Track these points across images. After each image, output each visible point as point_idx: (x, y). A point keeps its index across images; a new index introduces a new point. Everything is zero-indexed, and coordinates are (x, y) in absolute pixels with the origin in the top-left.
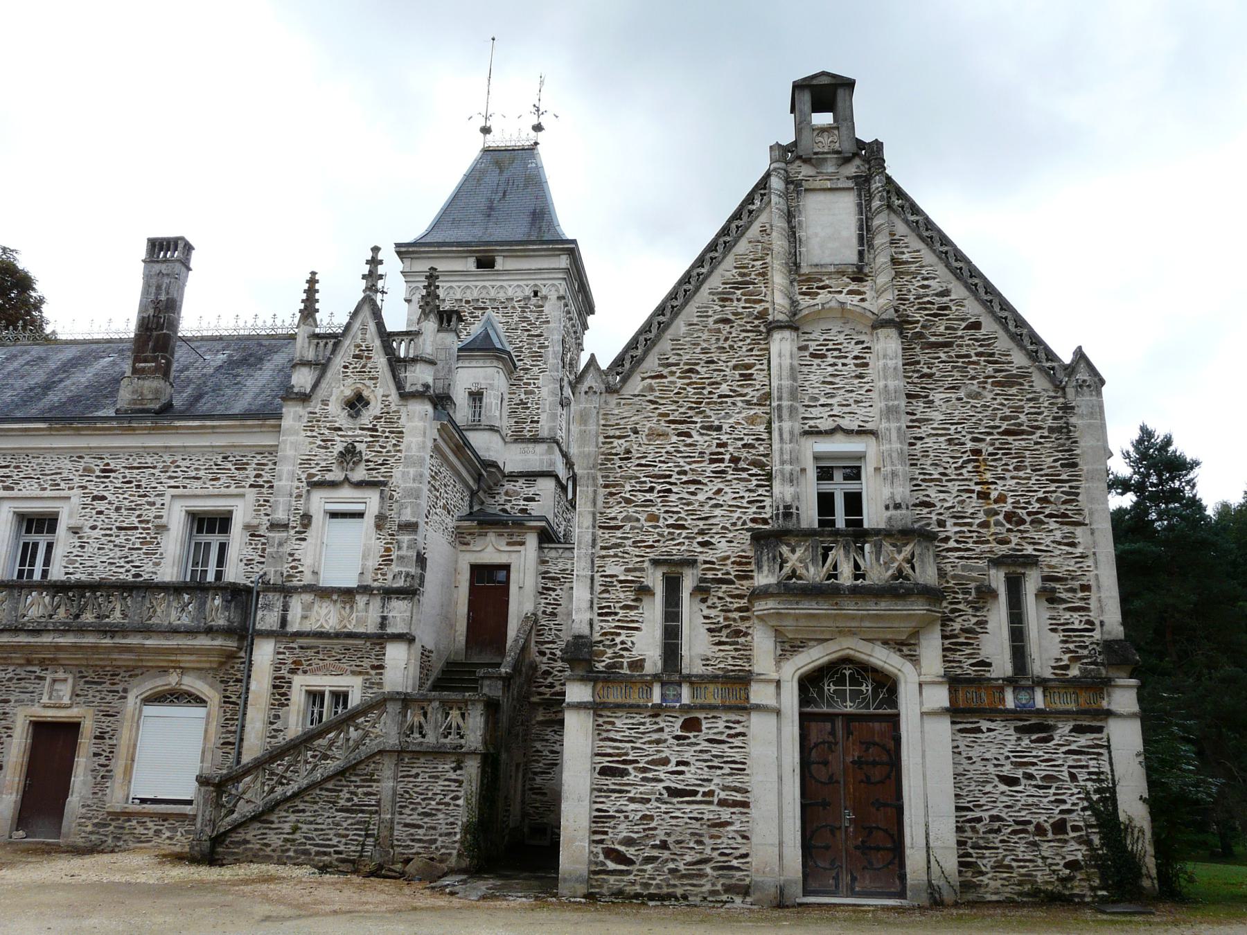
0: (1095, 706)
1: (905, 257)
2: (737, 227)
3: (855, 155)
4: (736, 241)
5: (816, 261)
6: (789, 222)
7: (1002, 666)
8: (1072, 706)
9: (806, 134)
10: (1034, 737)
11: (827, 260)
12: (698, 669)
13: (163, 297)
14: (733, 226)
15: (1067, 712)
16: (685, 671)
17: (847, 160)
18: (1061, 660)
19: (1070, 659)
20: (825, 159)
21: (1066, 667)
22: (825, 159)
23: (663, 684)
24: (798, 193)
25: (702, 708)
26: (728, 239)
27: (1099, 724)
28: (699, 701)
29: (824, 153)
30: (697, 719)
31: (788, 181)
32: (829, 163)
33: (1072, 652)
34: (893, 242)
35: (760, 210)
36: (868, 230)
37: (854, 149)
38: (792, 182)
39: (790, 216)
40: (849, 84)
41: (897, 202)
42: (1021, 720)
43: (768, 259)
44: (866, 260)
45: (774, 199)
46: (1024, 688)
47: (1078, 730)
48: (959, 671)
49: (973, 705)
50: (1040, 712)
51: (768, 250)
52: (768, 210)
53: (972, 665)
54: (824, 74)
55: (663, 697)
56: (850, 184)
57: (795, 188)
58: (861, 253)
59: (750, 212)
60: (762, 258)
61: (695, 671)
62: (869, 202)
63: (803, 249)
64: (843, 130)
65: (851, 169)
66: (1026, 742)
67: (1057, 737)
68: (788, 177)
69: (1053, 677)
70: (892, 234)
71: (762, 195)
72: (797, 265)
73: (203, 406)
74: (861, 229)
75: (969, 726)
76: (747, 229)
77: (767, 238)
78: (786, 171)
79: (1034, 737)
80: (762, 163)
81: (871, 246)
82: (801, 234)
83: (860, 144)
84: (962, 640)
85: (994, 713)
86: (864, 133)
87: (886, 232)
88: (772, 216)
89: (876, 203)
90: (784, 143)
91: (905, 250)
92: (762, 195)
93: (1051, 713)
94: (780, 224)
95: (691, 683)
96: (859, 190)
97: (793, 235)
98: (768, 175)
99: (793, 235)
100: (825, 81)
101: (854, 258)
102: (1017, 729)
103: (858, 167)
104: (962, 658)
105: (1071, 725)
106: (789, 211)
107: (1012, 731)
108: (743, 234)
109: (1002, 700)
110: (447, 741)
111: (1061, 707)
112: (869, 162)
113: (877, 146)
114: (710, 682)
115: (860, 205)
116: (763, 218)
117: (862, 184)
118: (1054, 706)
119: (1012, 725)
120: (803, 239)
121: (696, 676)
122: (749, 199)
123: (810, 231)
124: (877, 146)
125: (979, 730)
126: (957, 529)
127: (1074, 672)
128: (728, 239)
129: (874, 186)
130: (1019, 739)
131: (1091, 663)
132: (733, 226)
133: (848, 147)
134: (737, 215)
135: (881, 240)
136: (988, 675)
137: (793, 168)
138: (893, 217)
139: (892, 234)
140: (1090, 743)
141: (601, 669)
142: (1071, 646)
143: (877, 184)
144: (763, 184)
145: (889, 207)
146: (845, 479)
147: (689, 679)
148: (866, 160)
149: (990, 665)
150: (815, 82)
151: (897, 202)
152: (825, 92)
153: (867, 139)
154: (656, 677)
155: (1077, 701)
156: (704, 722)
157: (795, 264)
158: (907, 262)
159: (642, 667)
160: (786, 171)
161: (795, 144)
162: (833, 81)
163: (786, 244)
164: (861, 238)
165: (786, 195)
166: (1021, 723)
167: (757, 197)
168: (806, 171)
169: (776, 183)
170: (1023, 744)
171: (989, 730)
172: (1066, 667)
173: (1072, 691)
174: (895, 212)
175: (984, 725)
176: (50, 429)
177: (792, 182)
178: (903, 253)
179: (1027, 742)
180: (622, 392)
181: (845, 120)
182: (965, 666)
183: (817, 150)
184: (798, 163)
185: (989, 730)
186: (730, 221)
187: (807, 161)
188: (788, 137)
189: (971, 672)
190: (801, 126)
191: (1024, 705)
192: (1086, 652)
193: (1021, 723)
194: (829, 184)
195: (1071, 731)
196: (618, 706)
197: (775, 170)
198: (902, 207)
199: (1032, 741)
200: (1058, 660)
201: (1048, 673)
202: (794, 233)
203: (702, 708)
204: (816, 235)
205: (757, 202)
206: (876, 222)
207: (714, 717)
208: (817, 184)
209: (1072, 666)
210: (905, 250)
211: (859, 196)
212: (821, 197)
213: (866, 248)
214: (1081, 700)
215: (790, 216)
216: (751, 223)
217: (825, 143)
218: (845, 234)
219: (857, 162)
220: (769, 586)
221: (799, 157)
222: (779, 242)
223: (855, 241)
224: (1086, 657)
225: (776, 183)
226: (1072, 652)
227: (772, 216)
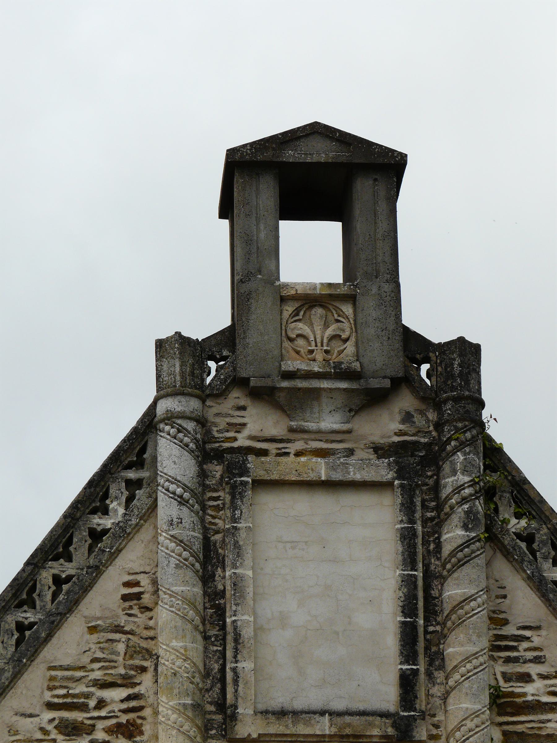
1: (533, 690)
2: (58, 581)
3: (406, 381)
4: (54, 623)
5: (279, 699)
6: (207, 579)
9: (262, 309)
11: (312, 699)
14: (46, 577)
17: (370, 400)
20: (314, 394)
22: (315, 393)
24: (236, 492)
26: (30, 616)
29: (309, 375)
31: (206, 451)
32: (326, 404)
34: (501, 645)
35: (124, 533)
36: (431, 611)
37: (396, 367)
38: (218, 455)
39: (210, 559)
40: (389, 167)
41: (516, 525)
43: (146, 683)
44: (421, 704)
45: (167, 509)
51: (144, 655)
52: (145, 534)
54: (317, 130)
56: (383, 471)
57: (228, 475)
58: (407, 683)
59: (96, 535)
60: (126, 681)
62: (435, 526)
63: (246, 665)
64: (369, 306)
65: (385, 425)
68: (208, 438)
70: (497, 620)
71: (133, 485)
72: (227, 713)
74: (408, 608)
76: (86, 589)
77: (141, 619)
78: (202, 422)
80: (132, 393)
81: (436, 659)
82: (241, 617)
83: (415, 346)
86: (428, 314)
87: (480, 620)
88: (156, 550)
89: (454, 535)
90: (199, 331)
91: (534, 669)
92: (133, 485)
94: (179, 585)
96: (408, 493)
97: (215, 619)
98: (148, 426)
99: (215, 619)
100: (320, 152)
101: (388, 697)
103: (407, 418)
106: (207, 545)
108: (73, 605)
112: (438, 406)
113: (464, 357)
115: (407, 537)
116: (132, 558)
117: (413, 470)
120: (247, 633)
122: (94, 497)
123: (268, 609)
124: (464, 357)
128: (30, 616)
129: (449, 482)
132: (46, 577)
133: (381, 359)
134: (56, 546)
135: (464, 645)
137: (222, 412)
138: (503, 569)
139: (497, 620)
143: (458, 475)
144: (135, 451)
145: (493, 536)
146: (517, 629)
148: (430, 398)
150: (290, 155)
151: (516, 525)
152: (322, 174)
153: (438, 334)
157: (221, 705)
158: (537, 707)
160: (202, 422)
161: (227, 339)
162: (344, 156)
163: (195, 647)
164: (408, 636)
165: (198, 497)
167: (118, 489)
168: (259, 423)
169: (172, 459)
174: (507, 554)
177: (218, 455)
178: (526, 678)
180: (296, 342)
181: (374, 262)
183: (291, 365)
184: (236, 396)
186: (36, 562)
187: (263, 395)
188: (208, 314)
190: (252, 266)
194: (321, 469)
197: (170, 418)
198: (529, 539)
202: (221, 612)
204: (283, 620)
205: (117, 509)
206: (454, 591)
208: (289, 467)
210: (534, 669)
211: (408, 508)
212: (300, 504)
213: (422, 667)
215: (210, 559)
216: (96, 571)
217: (314, 342)
218: (365, 620)
219: (406, 401)
221: (242, 383)
222: (176, 644)
223: (391, 643)
225: (172, 459)
227: (156, 550)
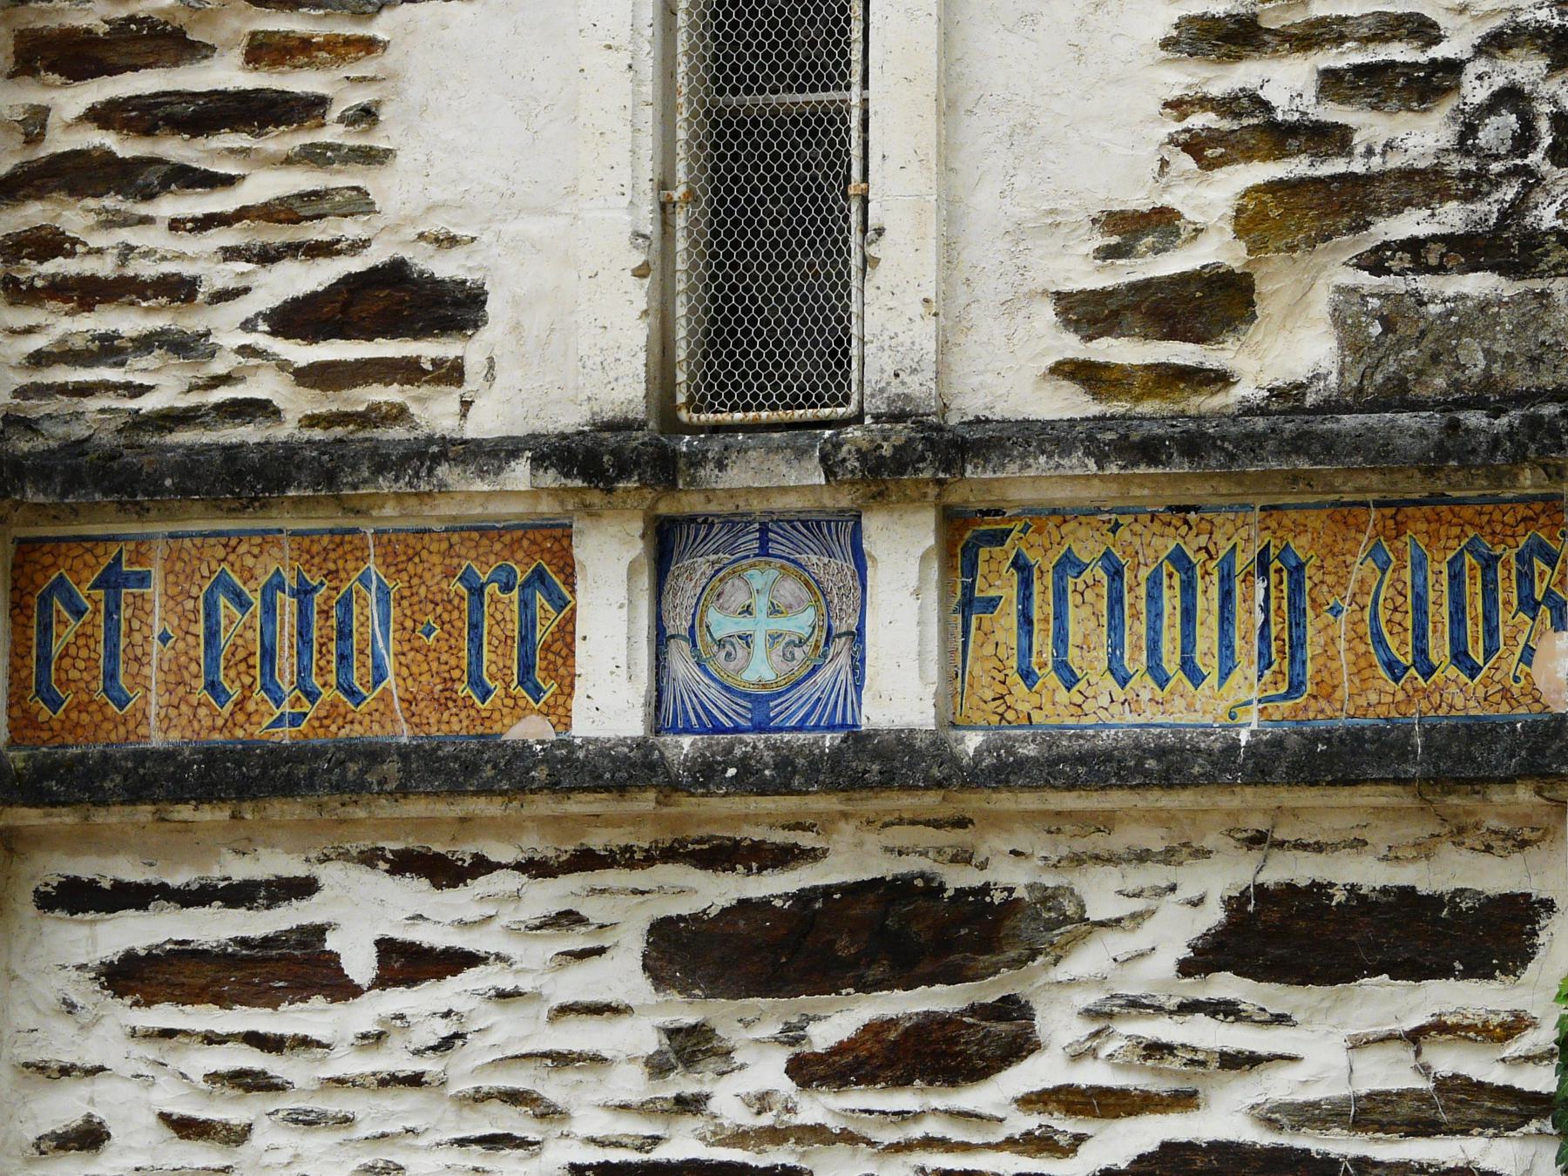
0: (1461, 696)
7: (572, 325)
8: (1232, 703)
10: (837, 1021)
15: (1166, 765)
18: (1161, 224)
19: (1250, 221)
21: (1218, 302)
27: (1496, 877)
33: (1281, 136)
42: (719, 856)
46: (766, 533)
47: (1284, 939)
48: (167, 387)
49: (266, 724)
50: (875, 767)
53: (295, 319)
66: (754, 1070)
67: (1059, 1024)
69: (1069, 404)
75: (213, 927)
79: (837, 1021)
84: (227, 74)
85: (449, 789)
93: (1003, 772)
102: (679, 952)
104: (200, 258)
105: (1214, 884)
107: (621, 974)
109: (546, 662)
111: (1115, 710)
118: (1051, 706)
119: (629, 908)
125: (305, 967)
127: (1291, 345)
130: (690, 1047)
131: (1469, 250)
136: (436, 413)
140: (1391, 1073)
142: (1287, 83)
149: (457, 308)
155: (1285, 651)
166: (715, 892)
170: (728, 1100)
171: (406, 963)
172: (1218, 302)
173: (1242, 539)
175: (361, 911)
176: (326, 15)
179: (767, 1070)
182: (226, 328)
185: (406, 963)
189: (282, 389)
191: (760, 707)
192: (1423, 135)
193: (715, 892)
195: (1201, 961)
199: (809, 1071)
200: (1132, 229)
201: (1013, 371)
209: (1276, 284)
214: (1332, 639)
220: (1518, 193)
224: (1423, 185)
226: (1281, 136)
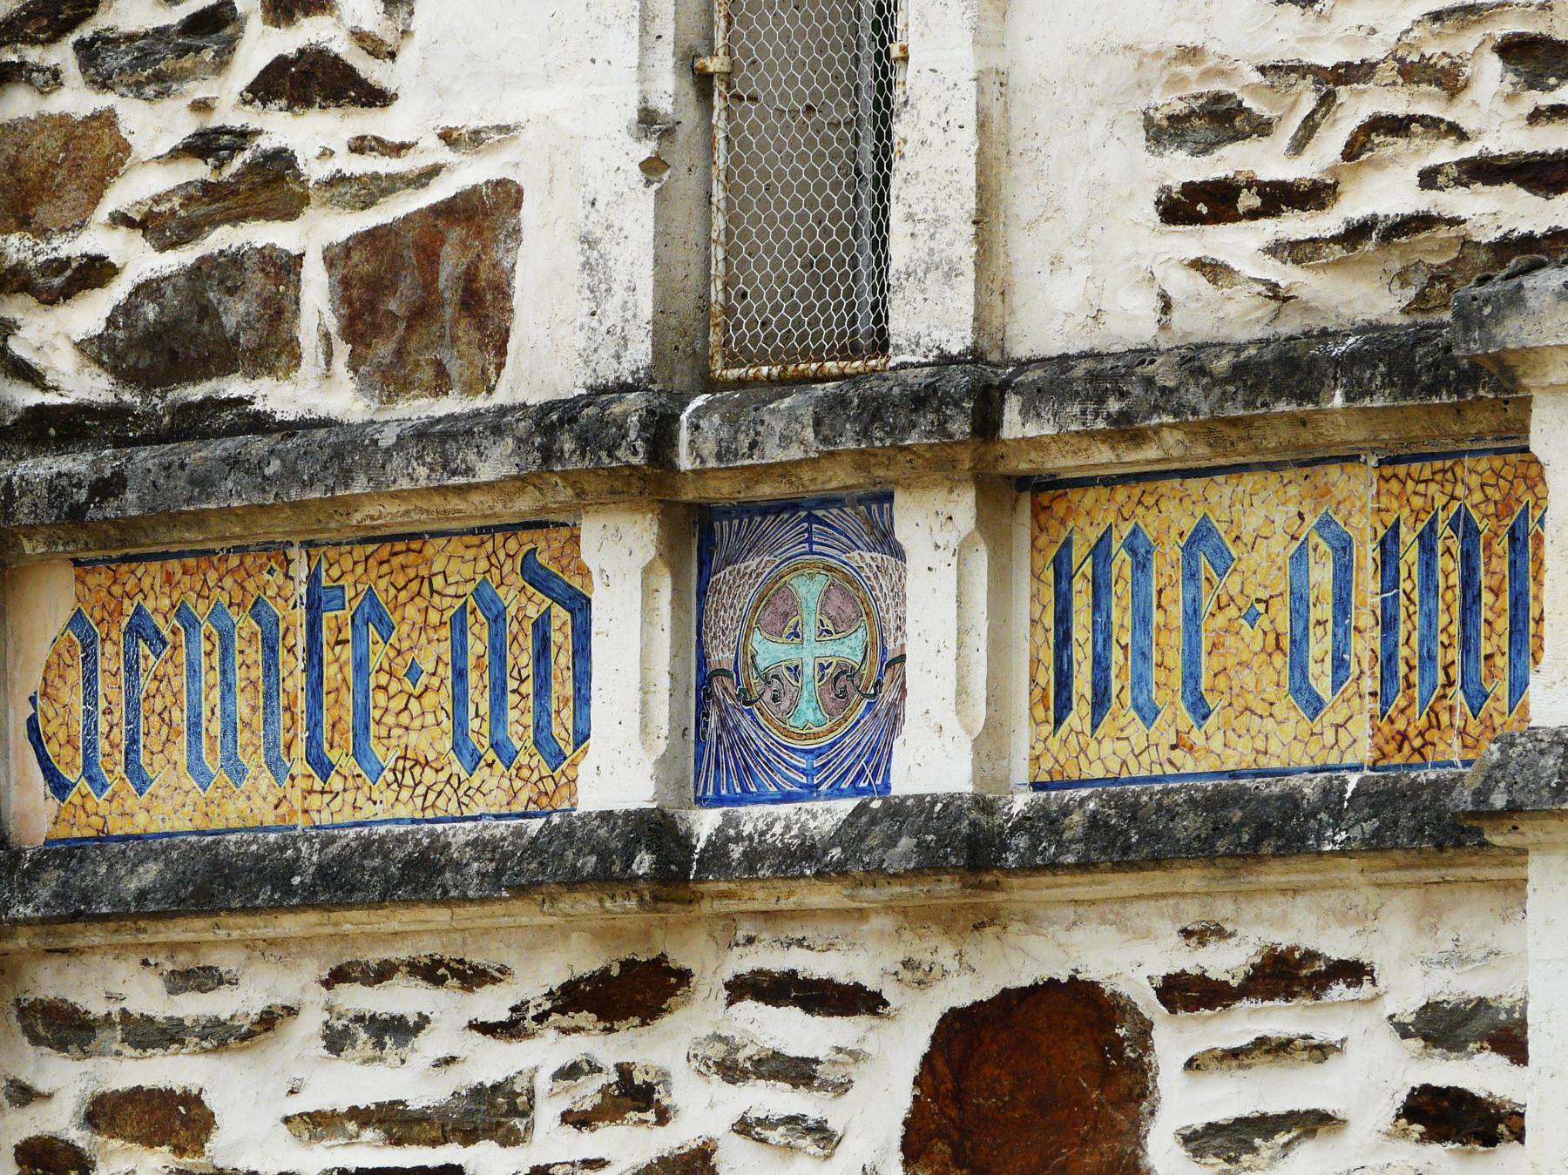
12: (1102, 272)
13: (484, 135)
16: (929, 319)
23: (701, 537)
25: (1130, 837)
28: (1123, 749)
30: (1082, 1007)
55: (714, 703)
61: (1047, 324)
73: (1036, 555)
95: (1018, 495)
110: (640, 450)
114: (1229, 454)
121: (1060, 380)
126: (254, 761)
141: (86, 385)
147: (964, 419)
154: (599, 447)
156: (1174, 1041)
159: (485, 306)
196: (224, 882)
203: (1130, 837)
207: (1282, 975)
